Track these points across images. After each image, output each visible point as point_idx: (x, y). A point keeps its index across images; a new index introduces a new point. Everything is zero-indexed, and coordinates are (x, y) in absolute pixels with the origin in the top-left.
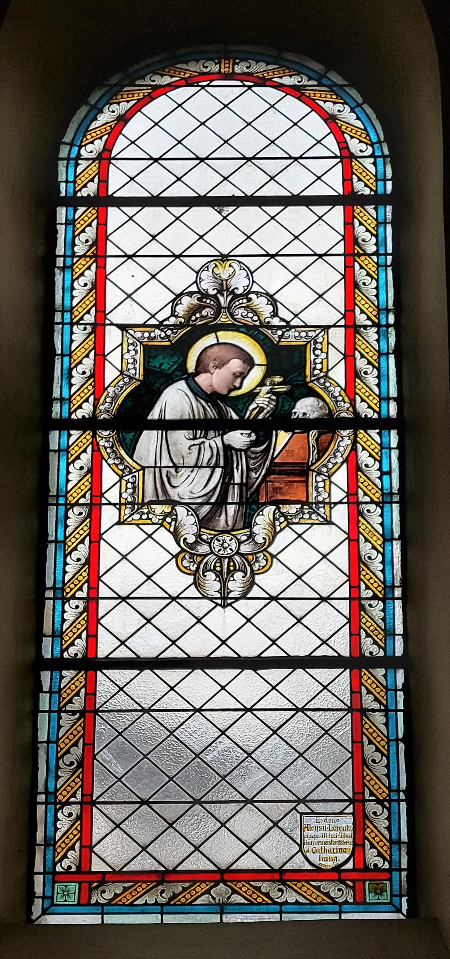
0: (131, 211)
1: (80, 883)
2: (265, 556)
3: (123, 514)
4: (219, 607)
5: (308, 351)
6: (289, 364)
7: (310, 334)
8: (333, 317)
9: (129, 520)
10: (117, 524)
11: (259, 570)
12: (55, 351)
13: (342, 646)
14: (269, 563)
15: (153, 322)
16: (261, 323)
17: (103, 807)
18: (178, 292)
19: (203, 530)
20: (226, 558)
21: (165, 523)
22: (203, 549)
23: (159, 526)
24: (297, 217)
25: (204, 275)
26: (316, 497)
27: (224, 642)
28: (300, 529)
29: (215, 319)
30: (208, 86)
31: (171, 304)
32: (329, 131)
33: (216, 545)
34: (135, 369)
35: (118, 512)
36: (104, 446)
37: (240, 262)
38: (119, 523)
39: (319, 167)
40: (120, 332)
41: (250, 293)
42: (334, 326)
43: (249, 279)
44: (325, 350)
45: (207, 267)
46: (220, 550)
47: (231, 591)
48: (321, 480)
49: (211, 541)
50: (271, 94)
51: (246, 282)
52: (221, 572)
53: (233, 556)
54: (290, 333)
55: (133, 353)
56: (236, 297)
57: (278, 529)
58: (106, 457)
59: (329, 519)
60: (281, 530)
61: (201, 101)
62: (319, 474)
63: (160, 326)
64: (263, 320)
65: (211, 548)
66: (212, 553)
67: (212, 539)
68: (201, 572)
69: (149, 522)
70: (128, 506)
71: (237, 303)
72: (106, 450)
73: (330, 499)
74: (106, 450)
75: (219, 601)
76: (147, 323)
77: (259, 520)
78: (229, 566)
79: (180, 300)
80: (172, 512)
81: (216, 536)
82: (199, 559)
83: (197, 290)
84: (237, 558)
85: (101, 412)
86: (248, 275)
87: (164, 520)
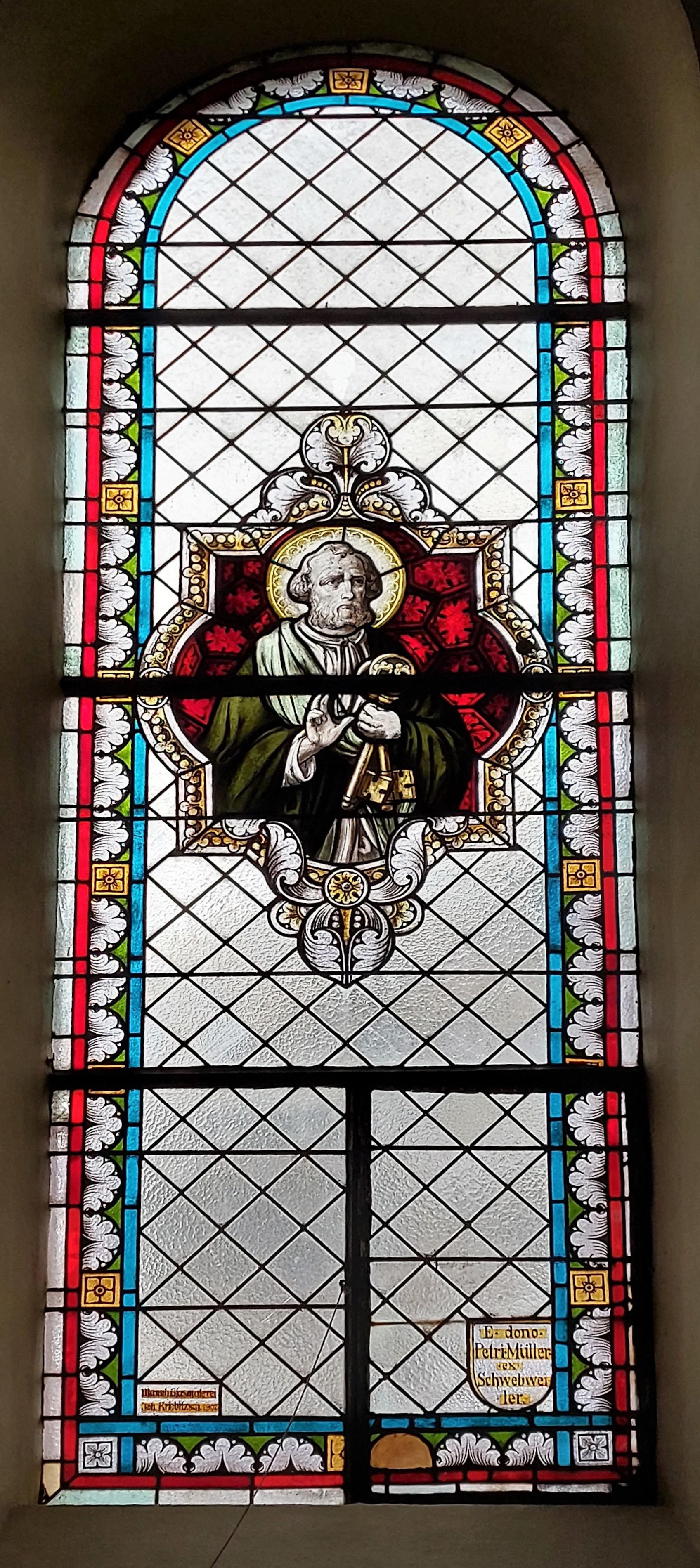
0: (194, 332)
1: (120, 1436)
2: (411, 905)
8: (521, 506)
9: (192, 847)
11: (402, 927)
15: (232, 518)
16: (403, 518)
18: (270, 468)
20: (348, 908)
22: (313, 895)
23: (240, 858)
24: (461, 341)
25: (312, 439)
28: (465, 859)
30: (317, 116)
31: (260, 488)
37: (371, 418)
41: (386, 469)
42: (522, 521)
43: (385, 446)
44: (507, 560)
50: (422, 130)
51: (381, 452)
52: (341, 930)
55: (197, 567)
56: (364, 478)
57: (430, 860)
59: (511, 842)
60: (436, 862)
64: (407, 512)
68: (308, 933)
69: (224, 850)
70: (190, 822)
73: (513, 807)
75: (338, 977)
77: (400, 844)
78: (353, 921)
80: (260, 832)
81: (331, 872)
87: (249, 846)
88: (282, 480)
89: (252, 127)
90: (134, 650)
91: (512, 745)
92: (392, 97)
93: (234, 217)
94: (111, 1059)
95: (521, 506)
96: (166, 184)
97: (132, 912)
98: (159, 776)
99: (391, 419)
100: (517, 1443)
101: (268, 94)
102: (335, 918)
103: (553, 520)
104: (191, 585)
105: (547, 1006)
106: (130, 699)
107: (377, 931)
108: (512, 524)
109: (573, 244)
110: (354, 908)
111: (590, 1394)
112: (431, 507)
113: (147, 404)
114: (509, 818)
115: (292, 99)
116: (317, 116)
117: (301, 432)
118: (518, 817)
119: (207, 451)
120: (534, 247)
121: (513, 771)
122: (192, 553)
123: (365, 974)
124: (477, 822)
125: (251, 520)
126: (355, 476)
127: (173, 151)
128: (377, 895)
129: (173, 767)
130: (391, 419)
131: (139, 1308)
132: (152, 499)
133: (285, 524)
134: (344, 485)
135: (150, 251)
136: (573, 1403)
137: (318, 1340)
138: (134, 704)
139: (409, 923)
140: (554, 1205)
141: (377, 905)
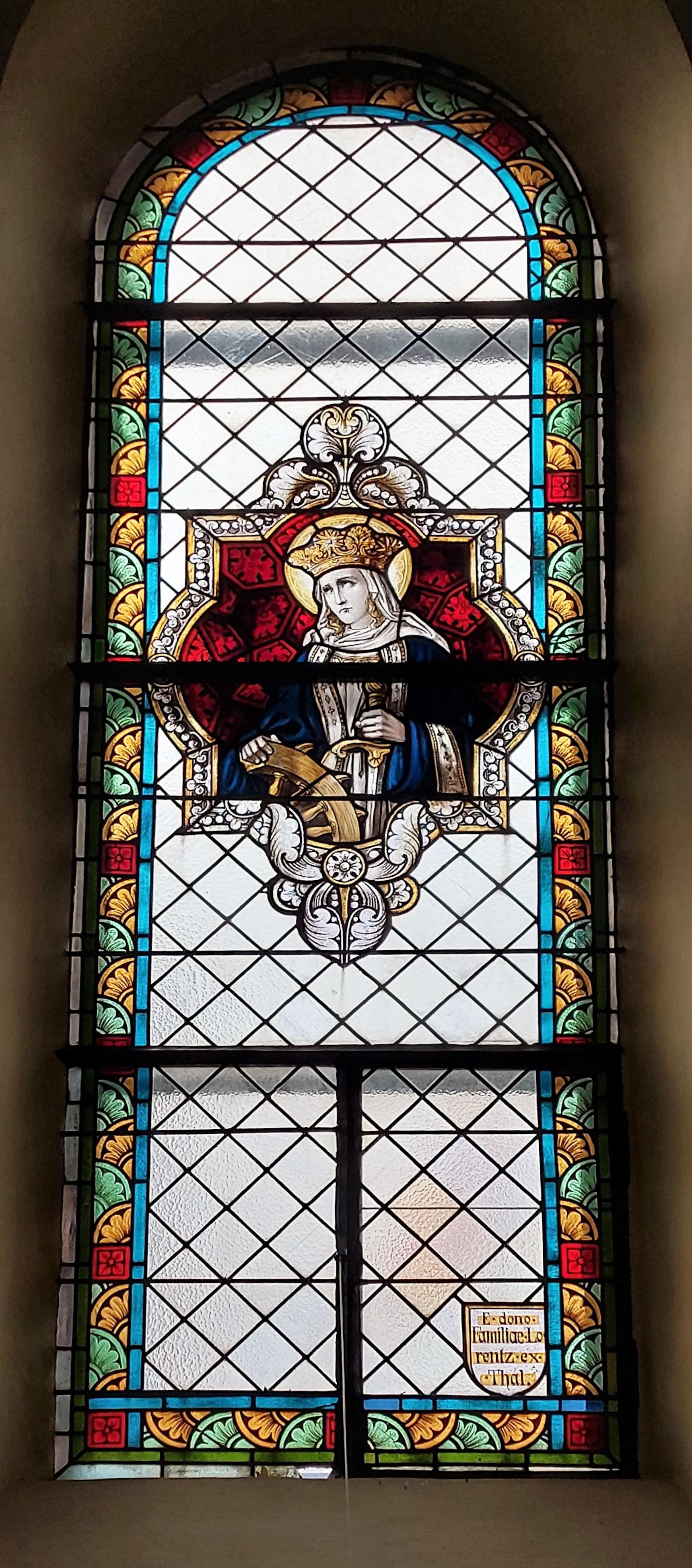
2: (407, 884)
3: (188, 814)
5: (473, 551)
6: (443, 569)
7: (476, 525)
10: (178, 832)
14: (415, 896)
15: (234, 506)
17: (161, 1138)
18: (272, 463)
20: (345, 887)
26: (485, 789)
27: (342, 1022)
28: (462, 841)
29: (331, 500)
30: (321, 126)
31: (263, 478)
34: (207, 579)
35: (180, 811)
36: (160, 701)
37: (366, 408)
38: (182, 831)
39: (492, 254)
40: (182, 522)
41: (384, 459)
42: (518, 509)
44: (499, 549)
45: (318, 417)
46: (336, 874)
48: (493, 760)
52: (339, 909)
53: (356, 883)
55: (202, 553)
56: (362, 466)
57: (426, 841)
63: (244, 512)
65: (322, 871)
71: (364, 476)
72: (162, 709)
74: (162, 709)
75: (337, 956)
77: (396, 826)
78: (350, 901)
79: (277, 472)
81: (330, 851)
82: (304, 889)
83: (302, 456)
85: (156, 653)
86: (381, 429)
88: (284, 471)
89: (260, 137)
93: (241, 219)
95: (513, 497)
98: (168, 754)
104: (196, 570)
107: (374, 909)
108: (502, 514)
110: (352, 886)
112: (427, 496)
114: (503, 803)
116: (321, 126)
117: (302, 424)
118: (511, 802)
119: (212, 445)
120: (539, 1138)
121: (506, 756)
124: (471, 806)
126: (355, 465)
129: (183, 748)
130: (388, 411)
137: (313, 1317)
139: (404, 904)
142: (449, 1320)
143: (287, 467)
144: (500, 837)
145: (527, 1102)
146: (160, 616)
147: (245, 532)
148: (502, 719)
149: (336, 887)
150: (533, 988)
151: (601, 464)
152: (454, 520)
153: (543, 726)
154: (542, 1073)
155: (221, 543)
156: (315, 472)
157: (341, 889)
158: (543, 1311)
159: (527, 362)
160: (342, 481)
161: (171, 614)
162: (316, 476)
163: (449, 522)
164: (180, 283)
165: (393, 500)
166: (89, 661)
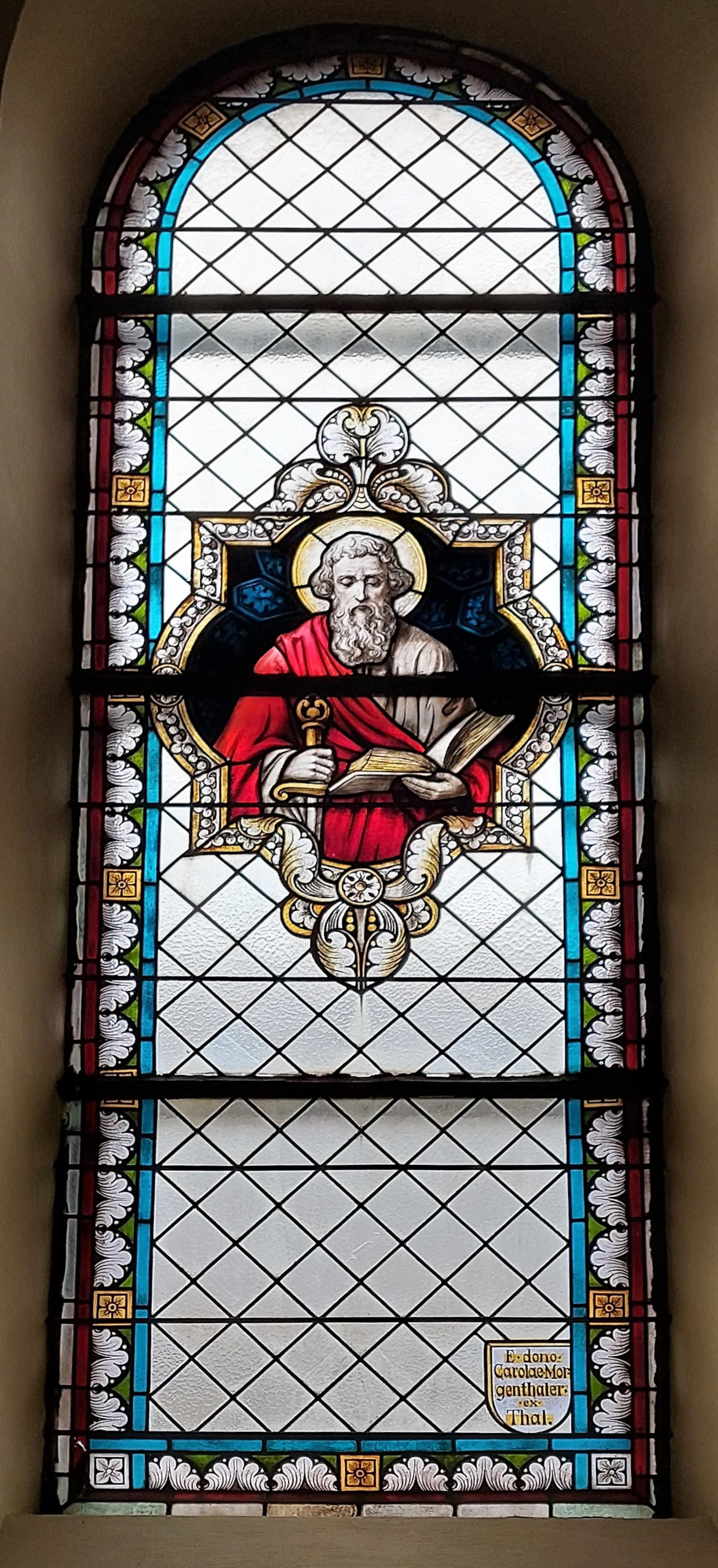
2: (427, 904)
4: (351, 992)
7: (503, 530)
8: (542, 501)
12: (86, 560)
13: (554, 1059)
15: (244, 508)
18: (285, 462)
19: (324, 862)
20: (362, 907)
21: (264, 851)
28: (484, 859)
29: (346, 504)
30: (338, 101)
32: (538, 182)
33: (345, 888)
34: (214, 585)
37: (388, 409)
39: (521, 244)
40: (188, 523)
41: (403, 461)
42: (545, 515)
44: (528, 556)
47: (372, 965)
48: (516, 781)
49: (339, 879)
50: (444, 117)
51: (398, 443)
52: (355, 933)
53: (374, 904)
54: (471, 527)
55: (210, 558)
56: (381, 468)
57: (446, 860)
58: (167, 742)
60: (452, 861)
61: (325, 131)
62: (514, 770)
66: (341, 899)
67: (342, 874)
69: (238, 849)
75: (353, 983)
76: (236, 510)
78: (367, 923)
79: (289, 473)
82: (318, 909)
84: (381, 907)
85: (160, 664)
86: (401, 431)
87: (263, 845)
88: (297, 471)
90: (145, 647)
91: (512, 577)
92: (412, 82)
93: (249, 203)
94: (123, 1064)
95: (542, 501)
96: (180, 170)
97: (145, 919)
99: (410, 412)
100: (533, 1467)
101: (286, 79)
102: (350, 920)
103: (575, 516)
104: (202, 576)
105: (565, 1013)
106: (142, 699)
107: (392, 933)
108: (530, 519)
109: (598, 234)
110: (369, 907)
111: (610, 1415)
112: (450, 499)
113: (160, 393)
115: (311, 83)
117: (318, 424)
119: (221, 444)
122: (203, 546)
123: (379, 981)
125: (264, 510)
126: (373, 466)
127: (188, 136)
128: (394, 892)
129: (191, 769)
130: (410, 412)
131: (152, 1320)
132: (164, 491)
133: (301, 514)
134: (366, 473)
135: (165, 236)
136: (591, 1425)
138: (147, 704)
140: (574, 1224)
141: (392, 903)
142: (470, 1359)
143: (301, 468)
144: (523, 856)
145: (553, 1135)
146: (164, 626)
147: (254, 536)
148: (526, 736)
149: (352, 908)
150: (565, 1244)
151: (633, 448)
152: (480, 525)
153: (569, 748)
154: (566, 316)
155: (229, 548)
156: (329, 473)
157: (356, 911)
158: (569, 1348)
159: (557, 359)
160: (358, 482)
161: (175, 622)
162: (332, 477)
163: (474, 525)
164: (185, 274)
165: (414, 504)
166: (89, 667)
